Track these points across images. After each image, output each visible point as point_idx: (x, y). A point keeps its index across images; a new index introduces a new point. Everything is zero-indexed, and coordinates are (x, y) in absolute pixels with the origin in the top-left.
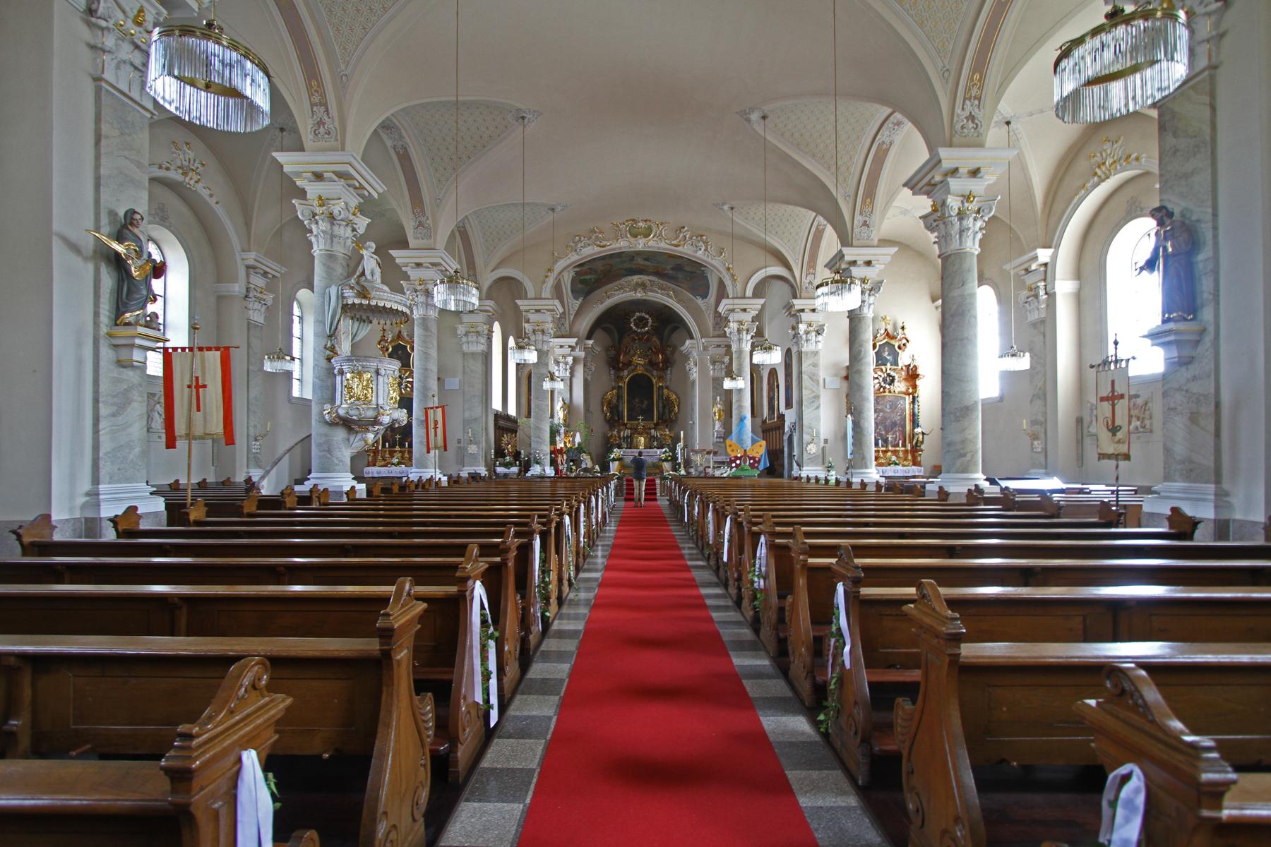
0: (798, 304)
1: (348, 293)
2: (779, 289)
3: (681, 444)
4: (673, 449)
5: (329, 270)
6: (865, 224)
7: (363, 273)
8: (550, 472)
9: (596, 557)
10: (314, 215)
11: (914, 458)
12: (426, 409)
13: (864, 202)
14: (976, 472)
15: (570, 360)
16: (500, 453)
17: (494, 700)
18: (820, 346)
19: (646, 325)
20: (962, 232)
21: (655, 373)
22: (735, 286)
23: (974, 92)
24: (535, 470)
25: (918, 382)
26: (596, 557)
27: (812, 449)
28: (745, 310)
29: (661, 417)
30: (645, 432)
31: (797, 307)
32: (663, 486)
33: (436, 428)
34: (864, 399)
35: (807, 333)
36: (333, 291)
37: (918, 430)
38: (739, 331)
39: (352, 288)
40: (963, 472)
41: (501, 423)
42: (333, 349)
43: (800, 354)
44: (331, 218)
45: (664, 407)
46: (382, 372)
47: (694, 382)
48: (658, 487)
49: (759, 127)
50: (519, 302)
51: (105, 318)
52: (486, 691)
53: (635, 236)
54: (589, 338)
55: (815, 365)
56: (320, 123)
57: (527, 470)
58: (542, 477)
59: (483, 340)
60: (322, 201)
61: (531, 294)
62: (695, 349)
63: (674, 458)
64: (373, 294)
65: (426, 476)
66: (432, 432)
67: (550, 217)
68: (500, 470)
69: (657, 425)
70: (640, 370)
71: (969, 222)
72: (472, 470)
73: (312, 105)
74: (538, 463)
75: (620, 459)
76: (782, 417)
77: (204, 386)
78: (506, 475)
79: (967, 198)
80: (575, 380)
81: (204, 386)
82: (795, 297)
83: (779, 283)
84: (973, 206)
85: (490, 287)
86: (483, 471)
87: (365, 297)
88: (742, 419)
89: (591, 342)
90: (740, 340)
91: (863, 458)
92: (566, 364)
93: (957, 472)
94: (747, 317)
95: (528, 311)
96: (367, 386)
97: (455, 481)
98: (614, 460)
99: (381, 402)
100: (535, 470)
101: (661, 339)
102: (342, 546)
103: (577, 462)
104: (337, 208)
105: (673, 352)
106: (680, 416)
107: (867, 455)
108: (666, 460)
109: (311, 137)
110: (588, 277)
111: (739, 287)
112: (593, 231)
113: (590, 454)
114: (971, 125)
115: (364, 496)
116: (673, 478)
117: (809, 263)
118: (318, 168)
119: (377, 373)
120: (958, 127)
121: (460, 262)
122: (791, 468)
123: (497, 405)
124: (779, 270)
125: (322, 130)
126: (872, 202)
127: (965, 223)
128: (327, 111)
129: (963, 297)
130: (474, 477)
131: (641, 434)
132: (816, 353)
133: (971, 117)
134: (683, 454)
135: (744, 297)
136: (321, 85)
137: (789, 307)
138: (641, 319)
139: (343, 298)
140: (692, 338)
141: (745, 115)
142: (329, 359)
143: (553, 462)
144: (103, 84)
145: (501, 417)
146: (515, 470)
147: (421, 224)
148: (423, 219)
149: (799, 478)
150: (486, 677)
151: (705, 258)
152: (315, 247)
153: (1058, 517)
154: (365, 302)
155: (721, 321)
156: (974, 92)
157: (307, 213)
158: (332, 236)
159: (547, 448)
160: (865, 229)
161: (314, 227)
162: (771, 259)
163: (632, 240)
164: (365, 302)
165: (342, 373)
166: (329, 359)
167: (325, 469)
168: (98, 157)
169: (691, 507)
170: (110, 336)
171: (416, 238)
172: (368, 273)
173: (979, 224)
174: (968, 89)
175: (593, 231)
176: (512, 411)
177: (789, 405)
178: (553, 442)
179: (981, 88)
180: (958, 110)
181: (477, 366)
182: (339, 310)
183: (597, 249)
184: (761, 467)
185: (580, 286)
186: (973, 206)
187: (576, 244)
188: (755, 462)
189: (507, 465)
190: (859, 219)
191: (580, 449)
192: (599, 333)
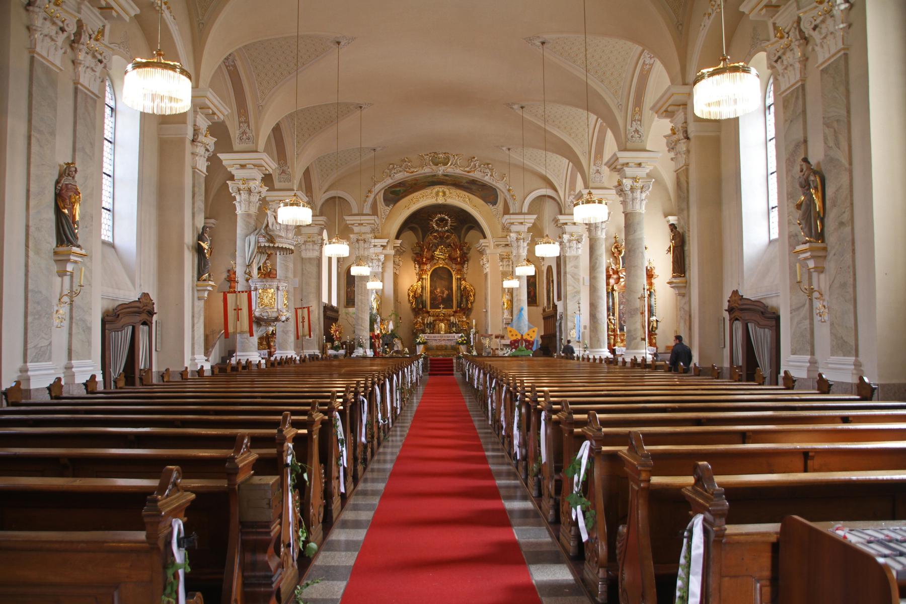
0: (562, 219)
1: (262, 240)
3: (473, 330)
4: (468, 336)
5: (247, 224)
6: (598, 171)
8: (370, 353)
10: (239, 190)
11: (650, 339)
13: (596, 157)
15: (382, 257)
18: (580, 251)
20: (633, 200)
21: (454, 266)
23: (637, 117)
24: (359, 352)
25: (653, 281)
29: (459, 305)
30: (445, 319)
31: (562, 221)
32: (459, 364)
33: (303, 322)
35: (570, 241)
36: (253, 238)
37: (654, 318)
38: (517, 240)
41: (328, 313)
44: (250, 191)
45: (462, 296)
46: (281, 288)
47: (486, 275)
48: (455, 365)
49: (520, 112)
50: (346, 218)
51: (196, 279)
54: (397, 237)
55: (576, 267)
56: (244, 133)
57: (351, 353)
58: (365, 357)
59: (317, 247)
61: (355, 211)
62: (490, 245)
63: (468, 342)
64: (278, 240)
66: (300, 325)
67: (372, 154)
69: (455, 312)
71: (638, 194)
72: (311, 352)
73: (240, 122)
74: (361, 346)
75: (424, 343)
76: (555, 307)
78: (336, 356)
82: (561, 214)
84: (639, 184)
85: (323, 205)
86: (317, 352)
87: (272, 242)
89: (399, 241)
90: (518, 247)
91: (598, 341)
92: (379, 260)
94: (524, 229)
98: (420, 343)
100: (359, 352)
101: (459, 237)
102: (55, 459)
103: (390, 345)
104: (252, 185)
108: (462, 343)
109: (238, 141)
110: (398, 189)
111: (517, 205)
112: (404, 161)
113: (400, 339)
114: (637, 135)
116: (465, 357)
117: (570, 187)
118: (243, 162)
119: (278, 289)
120: (629, 136)
121: (231, 108)
123: (325, 300)
125: (244, 137)
126: (641, 111)
128: (249, 126)
130: (313, 358)
131: (442, 321)
132: (577, 258)
133: (637, 131)
134: (474, 338)
135: (521, 213)
136: (246, 111)
137: (556, 221)
138: (442, 220)
140: (485, 237)
141: (510, 105)
142: (247, 280)
143: (372, 346)
144: (79, 86)
145: (328, 309)
146: (342, 352)
147: (284, 172)
151: (491, 181)
152: (238, 209)
153: (870, 399)
154: (271, 245)
155: (506, 229)
156: (637, 117)
161: (238, 197)
163: (434, 167)
164: (271, 245)
166: (247, 280)
167: (244, 350)
168: (193, 203)
170: (197, 286)
173: (644, 195)
174: (633, 115)
175: (404, 161)
176: (334, 303)
177: (559, 298)
178: (372, 329)
179: (641, 115)
180: (629, 127)
181: (314, 270)
183: (407, 174)
184: (534, 348)
185: (391, 195)
186: (639, 184)
187: (391, 170)
188: (529, 344)
189: (336, 348)
190: (593, 168)
191: (393, 335)
192: (409, 235)
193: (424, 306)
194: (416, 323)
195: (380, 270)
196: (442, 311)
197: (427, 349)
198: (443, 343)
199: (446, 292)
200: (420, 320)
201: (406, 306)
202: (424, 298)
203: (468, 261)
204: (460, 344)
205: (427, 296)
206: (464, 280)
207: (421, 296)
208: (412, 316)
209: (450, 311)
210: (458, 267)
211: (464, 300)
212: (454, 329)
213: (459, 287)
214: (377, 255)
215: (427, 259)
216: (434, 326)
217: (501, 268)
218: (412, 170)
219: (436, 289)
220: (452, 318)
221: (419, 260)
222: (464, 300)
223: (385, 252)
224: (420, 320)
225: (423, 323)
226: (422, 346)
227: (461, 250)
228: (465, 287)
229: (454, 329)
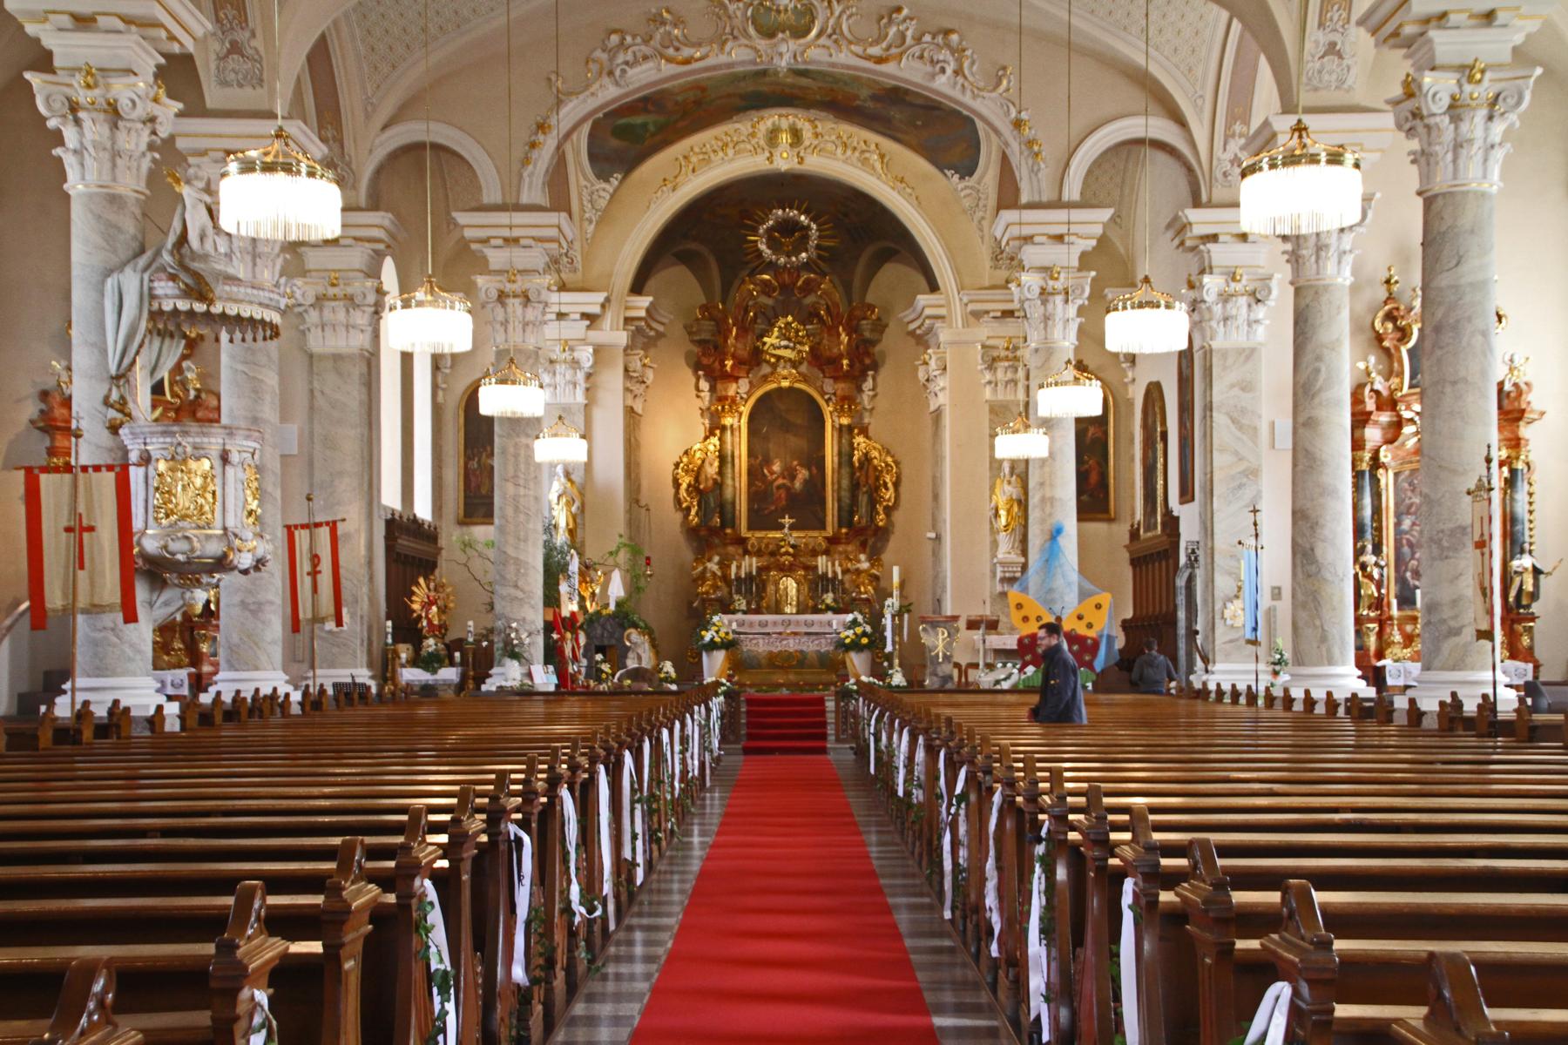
0: (1201, 220)
1: (164, 287)
2: (1156, 184)
3: (893, 603)
4: (876, 619)
6: (1332, 49)
7: (183, 239)
8: (545, 679)
9: (669, 892)
12: (290, 530)
14: (1344, 663)
15: (585, 355)
16: (408, 629)
17: (640, 859)
18: (1261, 332)
19: (801, 245)
20: (1457, 146)
21: (829, 386)
22: (1034, 171)
24: (507, 675)
25: (1525, 431)
26: (669, 892)
27: (1237, 614)
28: (1059, 238)
29: (845, 518)
30: (800, 563)
31: (1198, 230)
33: (314, 573)
34: (1328, 492)
35: (1225, 298)
36: (131, 281)
37: (1525, 562)
38: (1045, 294)
39: (173, 278)
40: (1454, 668)
41: (404, 542)
42: (122, 406)
43: (1208, 353)
44: (113, 113)
45: (855, 487)
46: (235, 457)
47: (937, 415)
52: (634, 850)
53: (769, 33)
54: (637, 288)
55: (1246, 387)
57: (483, 677)
58: (527, 693)
59: (361, 318)
60: (95, 75)
61: (492, 195)
64: (221, 289)
65: (266, 690)
66: (305, 584)
68: (411, 675)
69: (833, 541)
70: (785, 380)
71: (1475, 125)
72: (343, 675)
74: (515, 656)
75: (729, 645)
76: (1172, 523)
77: (91, 529)
78: (428, 690)
79: (1467, 71)
80: (598, 414)
81: (91, 529)
82: (1197, 203)
83: (1161, 157)
85: (379, 171)
86: (364, 676)
88: (1055, 534)
89: (644, 301)
92: (575, 364)
93: (1442, 669)
94: (1068, 256)
95: (485, 241)
96: (204, 488)
97: (313, 703)
98: (712, 646)
99: (230, 523)
100: (507, 675)
101: (847, 288)
103: (616, 653)
104: (121, 90)
105: (880, 327)
106: (898, 516)
107: (1333, 631)
108: (855, 646)
110: (638, 120)
111: (1046, 172)
113: (648, 631)
115: (177, 728)
116: (866, 690)
119: (225, 458)
122: (1190, 670)
123: (391, 497)
124: (1161, 128)
127: (1464, 127)
129: (1456, 288)
130: (349, 694)
131: (787, 570)
132: (1249, 354)
134: (897, 630)
135: (1058, 204)
137: (1179, 228)
138: (788, 227)
139: (152, 297)
140: (934, 287)
142: (114, 429)
143: (553, 654)
145: (401, 528)
146: (449, 674)
147: (236, 48)
148: (242, 36)
149: (1203, 693)
150: (634, 837)
152: (72, 173)
154: (200, 307)
157: (59, 104)
158: (115, 154)
159: (536, 616)
160: (1331, 62)
161: (70, 134)
162: (1137, 98)
163: (762, 44)
164: (200, 307)
165: (146, 460)
166: (114, 429)
167: (100, 671)
169: (878, 740)
171: (224, 83)
172: (193, 237)
176: (423, 509)
177: (1186, 495)
178: (551, 598)
181: (353, 395)
182: (143, 325)
183: (668, 69)
185: (614, 143)
187: (612, 53)
189: (429, 662)
190: (1316, 38)
191: (623, 617)
192: (676, 276)
193: (729, 519)
194: (702, 578)
195: (580, 398)
196: (788, 535)
197: (740, 665)
198: (792, 645)
199: (803, 474)
200: (713, 566)
201: (668, 522)
202: (728, 493)
203: (875, 367)
204: (848, 648)
205: (738, 486)
206: (864, 431)
207: (719, 485)
208: (688, 555)
209: (817, 537)
210: (842, 388)
211: (863, 499)
212: (829, 598)
213: (845, 455)
214: (568, 346)
215: (739, 362)
216: (762, 587)
217: (988, 393)
218: (687, 52)
219: (767, 462)
220: (822, 562)
221: (711, 362)
222: (863, 499)
223: (596, 336)
224: (713, 566)
225: (725, 578)
226: (720, 656)
227: (852, 330)
228: (867, 458)
229: (829, 598)
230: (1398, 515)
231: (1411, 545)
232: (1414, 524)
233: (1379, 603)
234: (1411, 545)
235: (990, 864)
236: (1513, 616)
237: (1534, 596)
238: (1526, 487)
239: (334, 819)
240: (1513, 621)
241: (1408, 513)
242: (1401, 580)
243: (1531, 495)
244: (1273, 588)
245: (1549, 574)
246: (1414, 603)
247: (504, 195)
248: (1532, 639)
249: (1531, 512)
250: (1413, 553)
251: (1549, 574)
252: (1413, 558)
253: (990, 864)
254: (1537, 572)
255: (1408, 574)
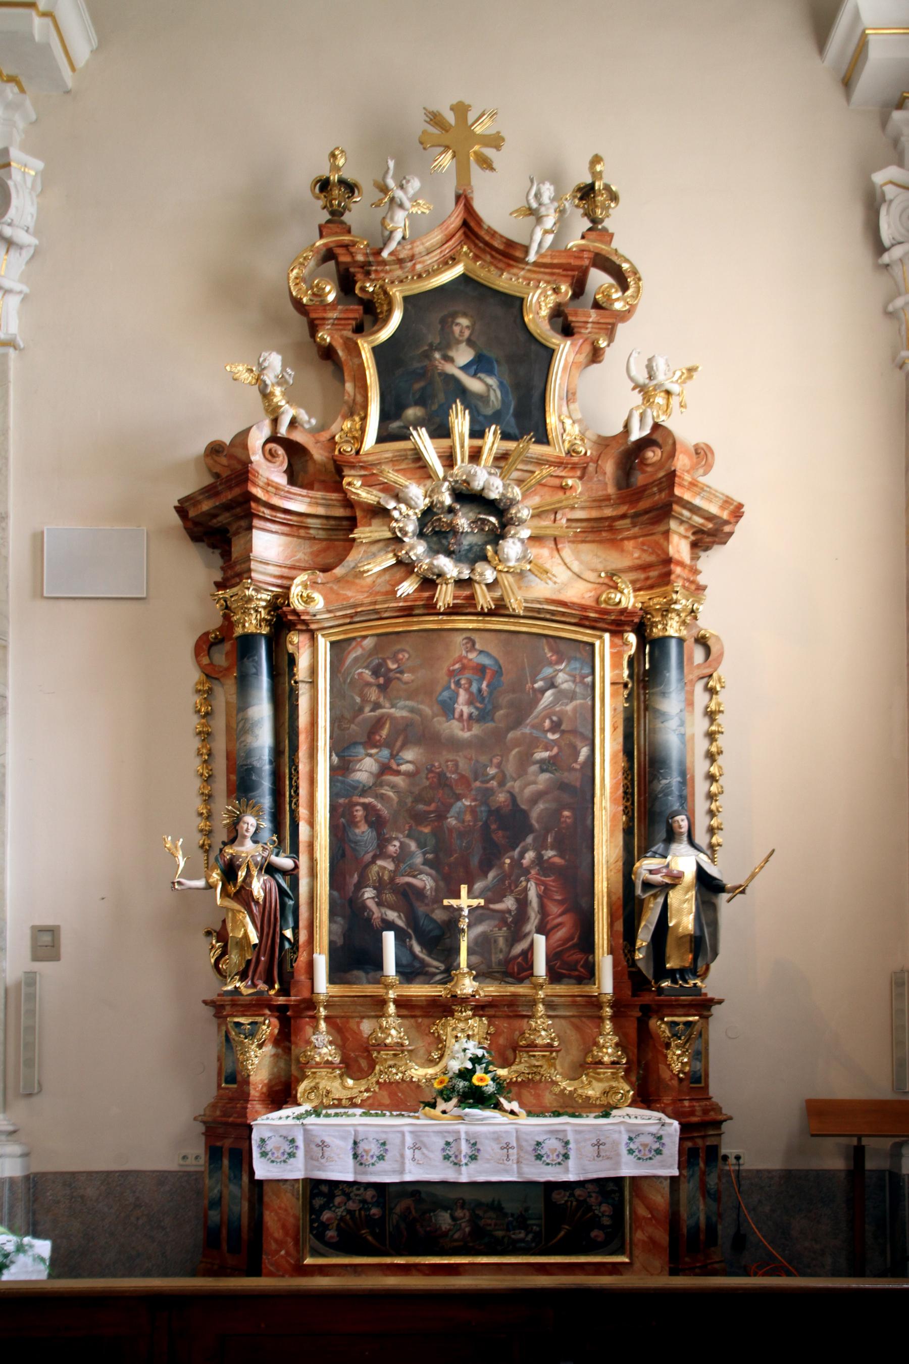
37: (684, 861)
230: (339, 746)
231: (376, 821)
232: (385, 769)
233: (276, 962)
234: (376, 821)
235: (888, 1246)
236: (647, 998)
237: (702, 945)
238: (701, 698)
239: (388, 1260)
240: (648, 1011)
241: (370, 741)
242: (346, 906)
243: (711, 715)
244: (38, 931)
245: (741, 890)
246: (378, 964)
247: (870, 1171)
248: (700, 1055)
249: (711, 757)
250: (382, 842)
251: (741, 890)
252: (381, 852)
253: (888, 1246)
254: (708, 885)
255: (369, 894)
